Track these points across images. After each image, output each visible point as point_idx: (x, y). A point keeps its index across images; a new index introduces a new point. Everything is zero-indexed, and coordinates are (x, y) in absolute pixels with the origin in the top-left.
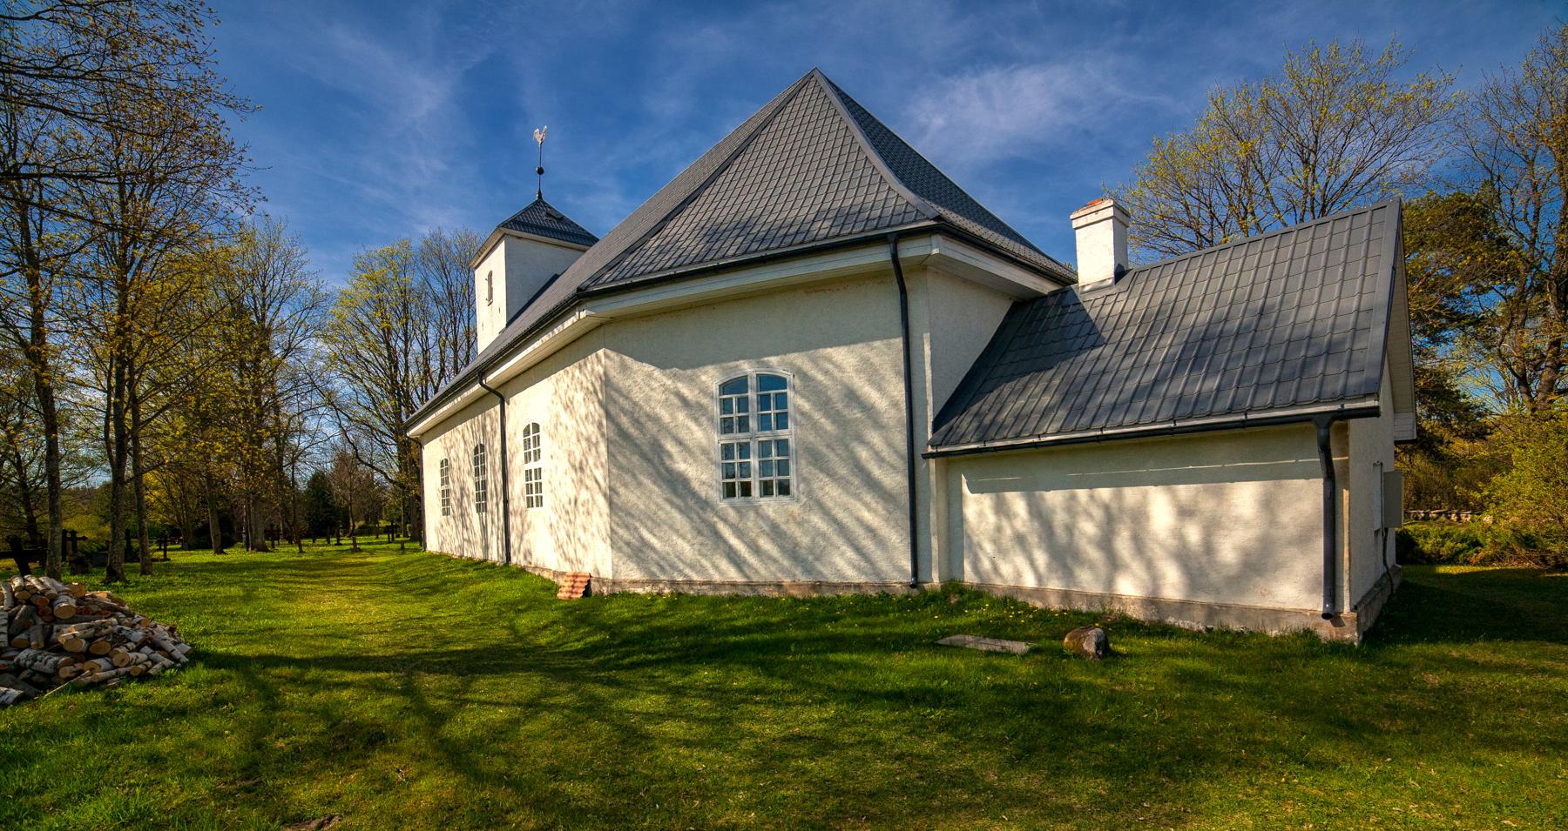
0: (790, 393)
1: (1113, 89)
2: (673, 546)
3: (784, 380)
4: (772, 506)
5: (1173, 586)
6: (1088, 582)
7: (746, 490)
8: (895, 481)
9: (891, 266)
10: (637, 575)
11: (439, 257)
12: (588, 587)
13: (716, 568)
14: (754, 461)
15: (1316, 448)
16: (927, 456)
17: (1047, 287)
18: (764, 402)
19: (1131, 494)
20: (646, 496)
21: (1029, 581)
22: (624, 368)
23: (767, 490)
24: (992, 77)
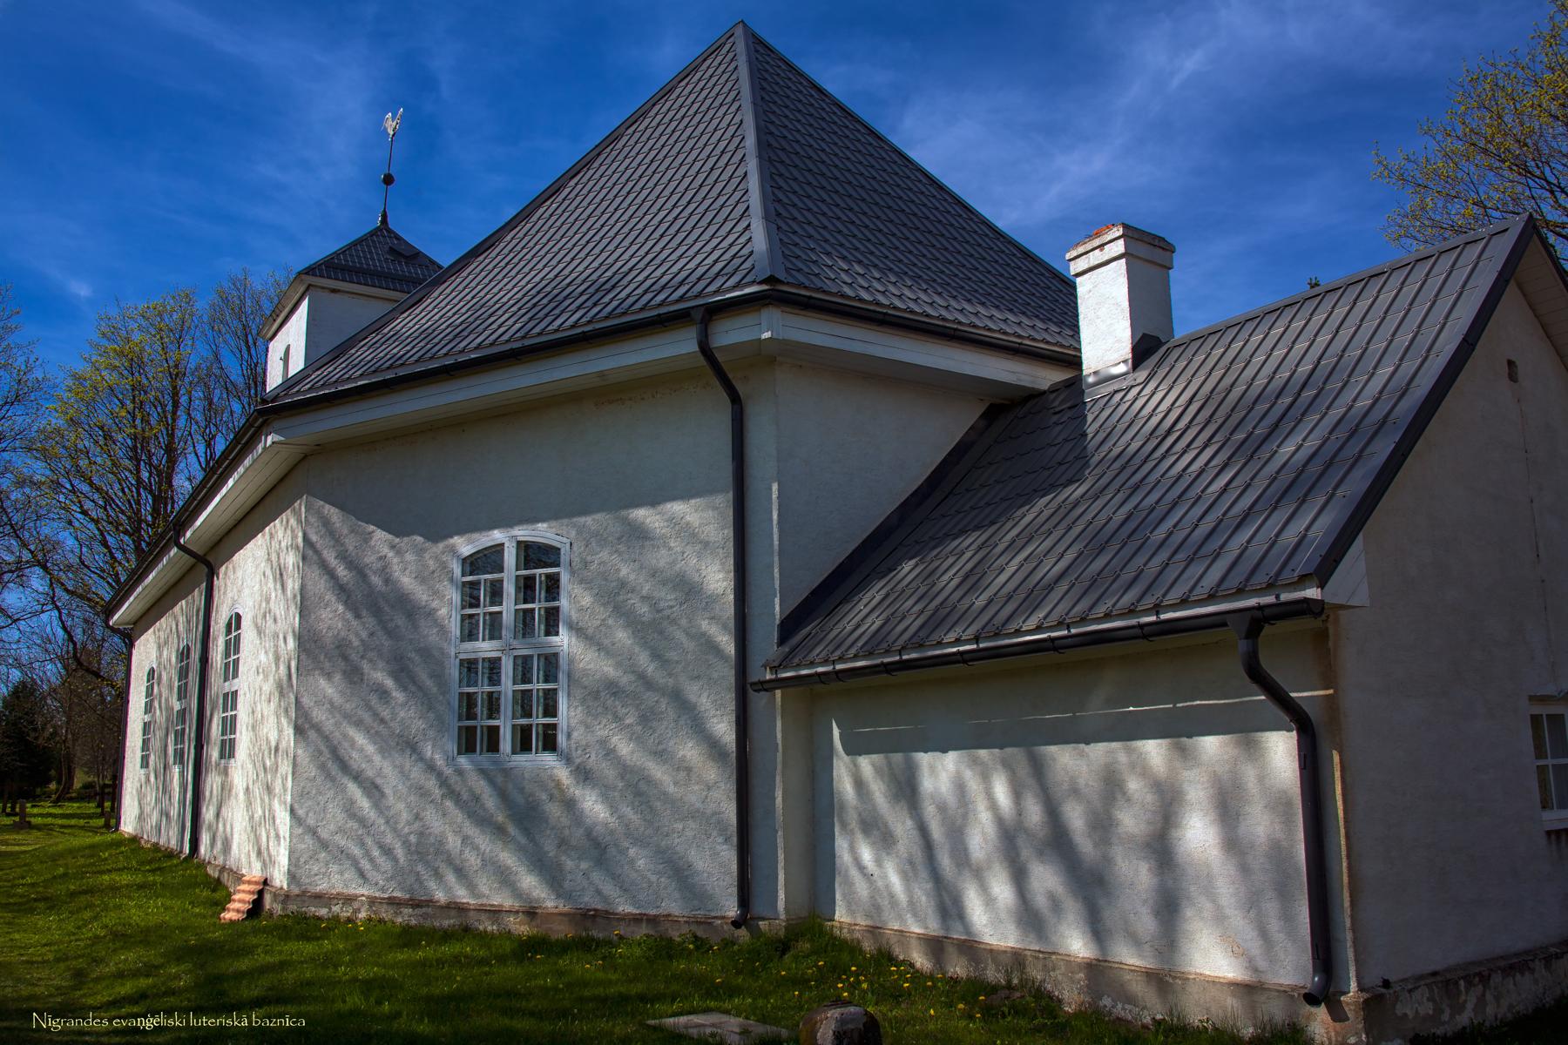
0: (565, 578)
2: (885, 877)
3: (556, 551)
7: (493, 745)
9: (702, 361)
11: (240, 313)
12: (258, 904)
14: (508, 686)
16: (764, 686)
17: (1046, 377)
18: (526, 588)
23: (524, 742)
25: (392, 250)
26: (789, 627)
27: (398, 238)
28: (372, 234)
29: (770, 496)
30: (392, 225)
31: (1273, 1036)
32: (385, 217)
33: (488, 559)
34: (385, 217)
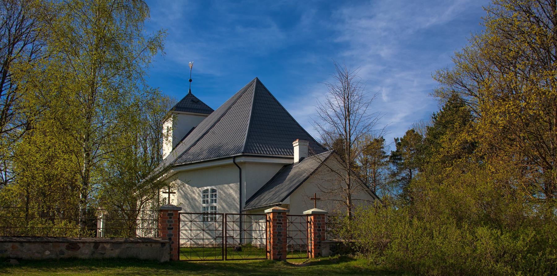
18: (212, 196)
25: (192, 101)
26: (248, 202)
27: (194, 96)
28: (187, 96)
29: (245, 184)
30: (192, 93)
31: (399, 145)
32: (190, 92)
33: (206, 191)
34: (190, 92)
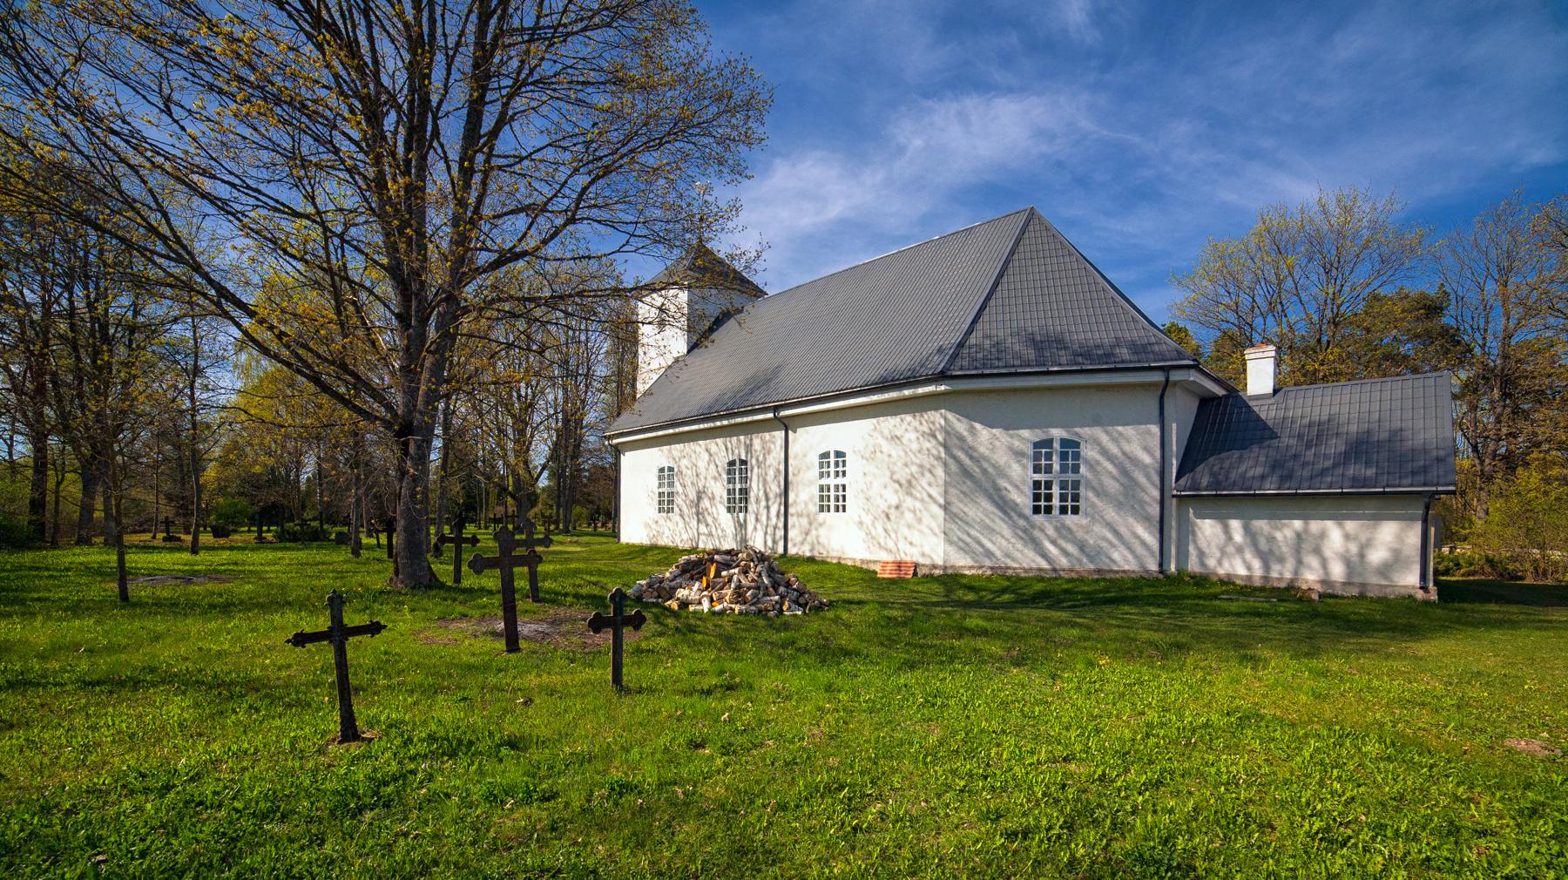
1: (1086, 124)
4: (1070, 519)
5: (1338, 572)
6: (1282, 573)
7: (1048, 510)
8: (1155, 510)
10: (970, 562)
13: (1066, 553)
15: (1422, 505)
19: (1315, 526)
20: (979, 510)
21: (1242, 571)
22: (972, 430)
24: (971, 103)
